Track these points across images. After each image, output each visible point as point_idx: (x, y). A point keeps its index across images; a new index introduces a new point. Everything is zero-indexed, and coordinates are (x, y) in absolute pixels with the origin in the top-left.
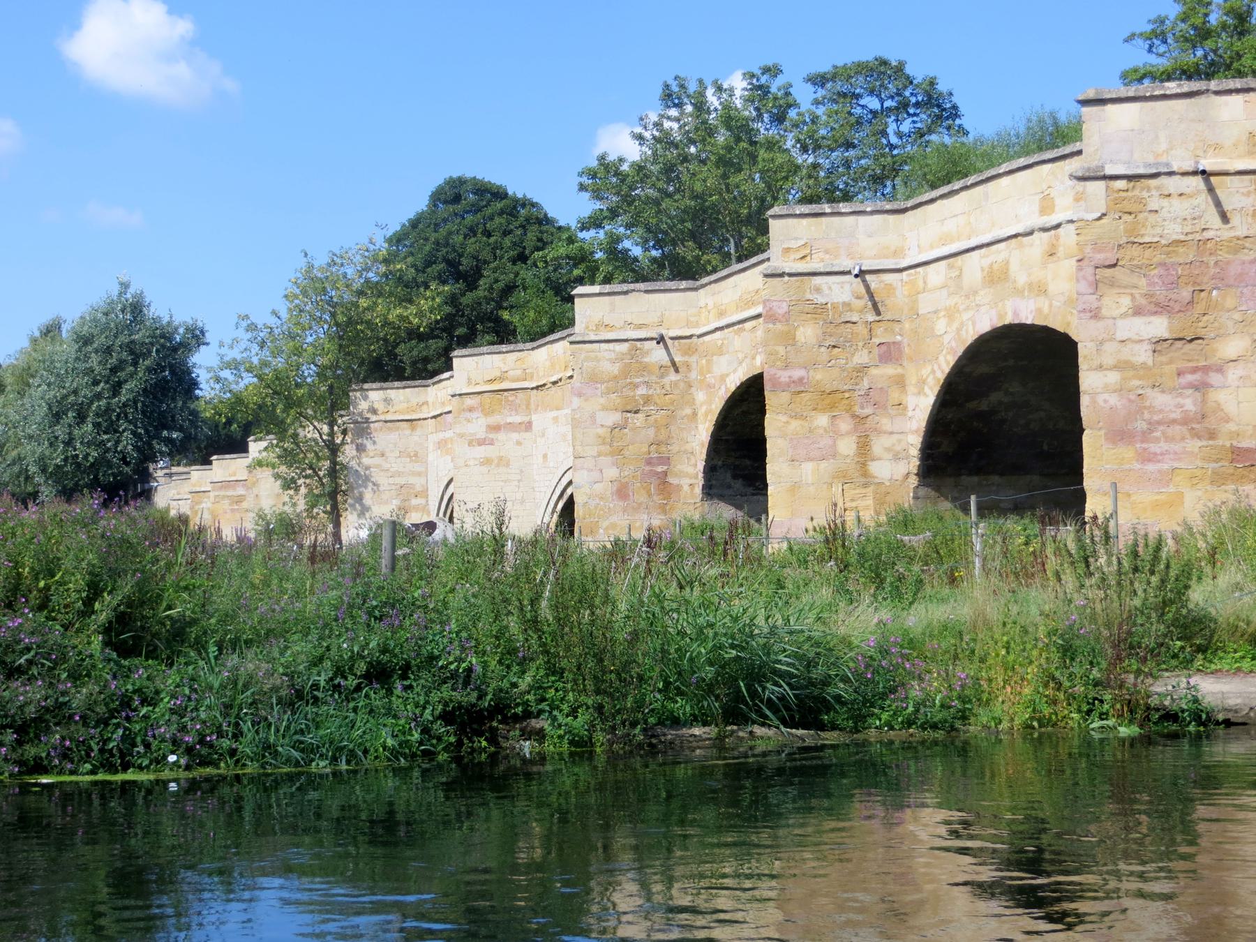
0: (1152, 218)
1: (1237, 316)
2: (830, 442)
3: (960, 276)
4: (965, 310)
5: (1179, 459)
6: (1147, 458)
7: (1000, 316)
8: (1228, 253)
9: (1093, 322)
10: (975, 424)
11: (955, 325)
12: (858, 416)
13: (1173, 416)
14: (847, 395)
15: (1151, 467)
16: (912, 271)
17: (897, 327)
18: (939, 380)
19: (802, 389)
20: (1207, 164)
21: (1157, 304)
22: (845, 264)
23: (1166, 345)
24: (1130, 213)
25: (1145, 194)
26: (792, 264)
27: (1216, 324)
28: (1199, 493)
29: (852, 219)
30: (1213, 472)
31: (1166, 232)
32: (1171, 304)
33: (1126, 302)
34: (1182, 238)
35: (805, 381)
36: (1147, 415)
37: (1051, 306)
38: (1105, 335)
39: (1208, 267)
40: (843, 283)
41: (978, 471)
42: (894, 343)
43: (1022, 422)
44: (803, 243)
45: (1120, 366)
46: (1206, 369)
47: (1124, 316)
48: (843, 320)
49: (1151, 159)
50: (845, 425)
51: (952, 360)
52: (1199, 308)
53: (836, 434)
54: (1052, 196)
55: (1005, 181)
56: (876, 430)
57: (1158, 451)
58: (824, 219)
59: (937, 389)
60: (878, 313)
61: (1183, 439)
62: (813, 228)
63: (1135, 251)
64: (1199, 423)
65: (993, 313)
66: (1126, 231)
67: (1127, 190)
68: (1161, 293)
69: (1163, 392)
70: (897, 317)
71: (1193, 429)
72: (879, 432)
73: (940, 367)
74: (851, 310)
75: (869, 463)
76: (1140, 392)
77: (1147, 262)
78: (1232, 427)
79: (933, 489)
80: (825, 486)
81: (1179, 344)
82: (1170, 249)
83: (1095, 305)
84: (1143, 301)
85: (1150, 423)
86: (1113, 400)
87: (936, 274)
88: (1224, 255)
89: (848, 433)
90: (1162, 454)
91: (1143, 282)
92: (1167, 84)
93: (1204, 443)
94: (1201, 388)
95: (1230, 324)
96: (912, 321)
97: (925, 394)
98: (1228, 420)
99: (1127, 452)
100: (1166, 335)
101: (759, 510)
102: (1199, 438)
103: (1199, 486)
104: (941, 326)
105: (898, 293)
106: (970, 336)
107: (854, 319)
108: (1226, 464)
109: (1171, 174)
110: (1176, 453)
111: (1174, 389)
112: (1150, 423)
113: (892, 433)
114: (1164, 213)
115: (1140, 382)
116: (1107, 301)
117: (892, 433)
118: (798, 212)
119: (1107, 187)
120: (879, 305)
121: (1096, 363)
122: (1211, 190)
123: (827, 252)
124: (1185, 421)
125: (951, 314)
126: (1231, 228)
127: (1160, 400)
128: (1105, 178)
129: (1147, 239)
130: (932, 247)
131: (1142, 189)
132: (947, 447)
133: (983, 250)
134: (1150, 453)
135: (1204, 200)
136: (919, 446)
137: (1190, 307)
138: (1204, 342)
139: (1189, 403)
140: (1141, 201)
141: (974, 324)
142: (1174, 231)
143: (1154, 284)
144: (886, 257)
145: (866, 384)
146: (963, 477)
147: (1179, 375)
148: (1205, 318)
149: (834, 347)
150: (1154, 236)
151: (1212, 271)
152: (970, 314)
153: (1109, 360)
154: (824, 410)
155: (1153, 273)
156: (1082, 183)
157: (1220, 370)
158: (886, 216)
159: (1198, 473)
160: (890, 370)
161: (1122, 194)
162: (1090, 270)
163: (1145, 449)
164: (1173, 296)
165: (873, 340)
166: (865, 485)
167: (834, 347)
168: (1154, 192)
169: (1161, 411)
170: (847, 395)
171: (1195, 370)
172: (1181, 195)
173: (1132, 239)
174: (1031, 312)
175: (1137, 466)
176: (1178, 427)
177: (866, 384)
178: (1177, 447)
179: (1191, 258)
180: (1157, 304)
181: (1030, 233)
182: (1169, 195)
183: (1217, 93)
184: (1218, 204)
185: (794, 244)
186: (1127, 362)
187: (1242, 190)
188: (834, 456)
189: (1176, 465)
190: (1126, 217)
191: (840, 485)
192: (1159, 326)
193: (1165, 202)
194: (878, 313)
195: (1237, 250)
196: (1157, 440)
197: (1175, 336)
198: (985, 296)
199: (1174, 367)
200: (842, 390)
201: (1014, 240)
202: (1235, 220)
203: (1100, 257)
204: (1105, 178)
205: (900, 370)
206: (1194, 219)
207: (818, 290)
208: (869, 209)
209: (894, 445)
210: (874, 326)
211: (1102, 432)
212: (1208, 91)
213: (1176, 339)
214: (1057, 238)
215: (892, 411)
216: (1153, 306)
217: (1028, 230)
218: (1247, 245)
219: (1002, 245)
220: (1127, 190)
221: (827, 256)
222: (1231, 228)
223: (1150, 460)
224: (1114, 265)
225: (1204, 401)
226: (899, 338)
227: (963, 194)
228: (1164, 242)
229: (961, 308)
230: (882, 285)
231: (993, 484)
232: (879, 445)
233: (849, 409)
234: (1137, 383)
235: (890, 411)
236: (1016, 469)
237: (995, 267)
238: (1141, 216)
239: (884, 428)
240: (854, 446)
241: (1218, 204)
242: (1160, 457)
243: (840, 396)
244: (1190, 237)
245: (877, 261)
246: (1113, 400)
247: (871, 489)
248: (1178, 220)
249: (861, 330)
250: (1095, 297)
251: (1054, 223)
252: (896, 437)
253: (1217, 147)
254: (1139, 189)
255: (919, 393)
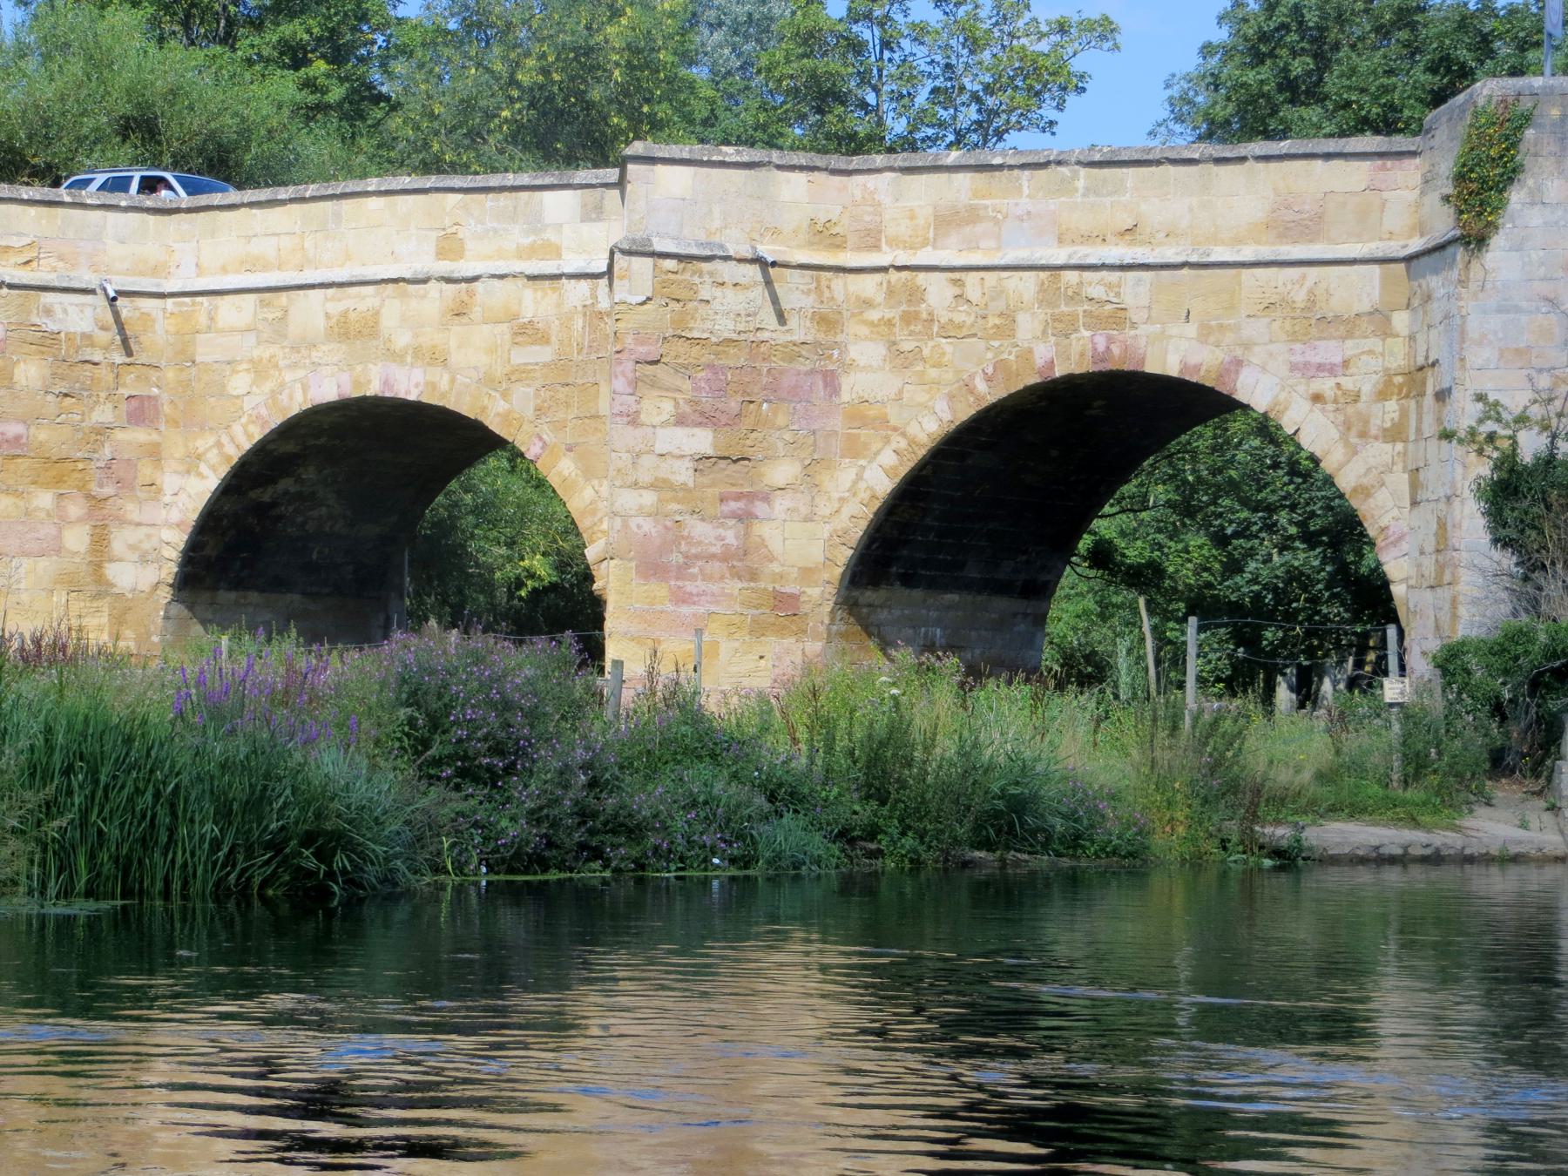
0: (703, 309)
1: (788, 436)
2: (54, 531)
3: (283, 319)
4: (289, 366)
5: (717, 602)
6: (681, 598)
7: (357, 384)
8: (783, 360)
9: (630, 428)
10: (250, 519)
11: (268, 386)
12: (94, 497)
13: (713, 550)
14: (80, 466)
15: (685, 610)
16: (187, 300)
17: (154, 375)
18: (229, 458)
19: (19, 452)
20: (768, 251)
21: (702, 414)
22: (87, 279)
23: (708, 463)
24: (678, 301)
25: (696, 280)
26: (9, 270)
27: (765, 444)
28: (736, 644)
29: (99, 213)
30: (753, 621)
31: (717, 327)
32: (717, 414)
33: (668, 407)
34: (734, 336)
35: (24, 440)
36: (684, 548)
37: (453, 380)
38: (643, 446)
39: (760, 374)
40: (83, 305)
41: (238, 585)
42: (149, 397)
43: (299, 519)
44: (28, 241)
45: (658, 485)
46: (751, 497)
47: (665, 424)
48: (80, 358)
49: (703, 237)
50: (75, 509)
51: (258, 434)
52: (747, 423)
53: (63, 521)
54: (460, 235)
55: (374, 203)
56: (117, 518)
57: (695, 591)
58: (60, 211)
59: (224, 470)
60: (129, 353)
61: (722, 578)
62: (44, 222)
63: (681, 347)
64: (741, 560)
65: (345, 379)
66: (673, 321)
67: (676, 273)
68: (706, 400)
69: (703, 520)
70: (154, 361)
71: (734, 567)
72: (123, 522)
73: (232, 439)
74: (92, 345)
75: (106, 565)
76: (678, 518)
77: (694, 362)
78: (775, 567)
79: (187, 607)
80: (44, 594)
81: (723, 463)
82: (720, 348)
83: (634, 407)
84: (688, 409)
85: (687, 557)
86: (648, 526)
87: (233, 312)
88: (778, 363)
89: (79, 520)
90: (698, 595)
91: (687, 385)
92: (724, 149)
93: (745, 585)
94: (746, 518)
95: (780, 444)
96: (181, 370)
97: (199, 475)
98: (771, 558)
99: (659, 590)
100: (710, 452)
101: (593, 651)
102: (740, 578)
103: (736, 636)
104: (239, 383)
105: (158, 327)
106: (296, 403)
107: (96, 359)
108: (768, 611)
109: (727, 258)
110: (713, 595)
111: (716, 518)
112: (687, 557)
113: (139, 524)
114: (715, 305)
115: (679, 507)
116: (647, 405)
117: (139, 524)
118: (26, 197)
119: (655, 265)
120: (132, 341)
121: (631, 479)
122: (768, 283)
123: (61, 258)
124: (725, 557)
125: (260, 370)
126: (788, 331)
127: (700, 530)
128: (653, 254)
129: (696, 334)
130: (224, 270)
131: (694, 273)
132: (211, 551)
133: (331, 291)
134: (685, 593)
135: (759, 294)
136: (182, 546)
137: (737, 420)
138: (750, 464)
139: (731, 537)
140: (691, 287)
141: (305, 389)
142: (725, 327)
143: (699, 389)
144: (142, 274)
145: (107, 452)
146: (221, 592)
147: (722, 501)
148: (754, 435)
149: (66, 395)
150: (703, 331)
151: (765, 380)
152: (300, 373)
153: (645, 477)
154: (46, 486)
155: (700, 375)
156: (627, 258)
157: (766, 499)
158: (145, 216)
159: (736, 619)
160: (141, 435)
161: (671, 276)
162: (630, 365)
163: (679, 587)
164: (720, 406)
165: (121, 391)
166: (98, 596)
167: (66, 395)
168: (706, 278)
169: (700, 543)
170: (80, 466)
171: (739, 497)
172: (735, 285)
173: (679, 332)
174: (417, 385)
175: (670, 607)
176: (718, 564)
177: (107, 452)
178: (714, 588)
179: (742, 362)
180: (702, 414)
181: (425, 281)
182: (723, 284)
183: (779, 167)
184: (775, 301)
185: (16, 242)
186: (665, 481)
187: (801, 287)
188: (58, 551)
189: (713, 608)
190: (674, 305)
191: (64, 593)
192: (702, 440)
193: (718, 292)
194: (129, 353)
195: (792, 358)
196: (693, 578)
197: (719, 454)
198: (330, 353)
199: (716, 491)
200: (75, 458)
201: (390, 286)
202: (793, 322)
203: (643, 351)
204: (653, 254)
205: (155, 437)
206: (749, 315)
207: (48, 312)
208: (123, 204)
209: (140, 542)
210: (123, 370)
211: (633, 564)
212: (770, 162)
213: (720, 458)
214: (471, 294)
215: (142, 494)
216: (697, 415)
217: (420, 276)
218: (804, 353)
219: (370, 289)
220: (676, 273)
221: (61, 264)
222: (788, 331)
223: (684, 602)
224: (657, 362)
225: (747, 534)
226: (155, 391)
227: (294, 208)
228: (714, 339)
229: (282, 363)
230: (137, 314)
231: (250, 604)
232: (120, 540)
233: (82, 487)
234: (674, 506)
235: (139, 494)
236: (278, 585)
237: (352, 316)
238: (690, 305)
239: (129, 517)
240: (87, 539)
241: (775, 301)
242: (696, 599)
243: (71, 466)
244: (743, 337)
245: (131, 279)
246: (648, 526)
247: (104, 604)
248: (732, 315)
249: (105, 374)
250: (633, 398)
251: (470, 274)
252: (145, 530)
253: (776, 232)
254: (688, 274)
255: (188, 472)
